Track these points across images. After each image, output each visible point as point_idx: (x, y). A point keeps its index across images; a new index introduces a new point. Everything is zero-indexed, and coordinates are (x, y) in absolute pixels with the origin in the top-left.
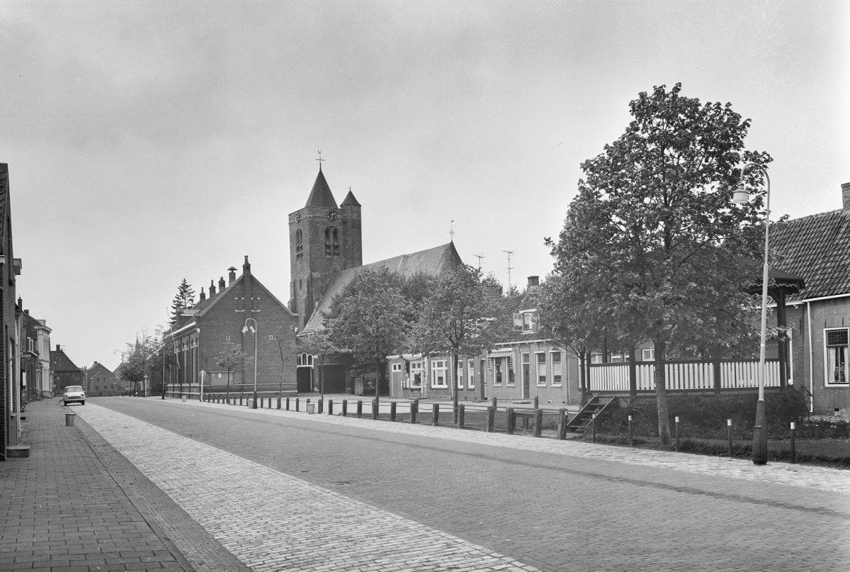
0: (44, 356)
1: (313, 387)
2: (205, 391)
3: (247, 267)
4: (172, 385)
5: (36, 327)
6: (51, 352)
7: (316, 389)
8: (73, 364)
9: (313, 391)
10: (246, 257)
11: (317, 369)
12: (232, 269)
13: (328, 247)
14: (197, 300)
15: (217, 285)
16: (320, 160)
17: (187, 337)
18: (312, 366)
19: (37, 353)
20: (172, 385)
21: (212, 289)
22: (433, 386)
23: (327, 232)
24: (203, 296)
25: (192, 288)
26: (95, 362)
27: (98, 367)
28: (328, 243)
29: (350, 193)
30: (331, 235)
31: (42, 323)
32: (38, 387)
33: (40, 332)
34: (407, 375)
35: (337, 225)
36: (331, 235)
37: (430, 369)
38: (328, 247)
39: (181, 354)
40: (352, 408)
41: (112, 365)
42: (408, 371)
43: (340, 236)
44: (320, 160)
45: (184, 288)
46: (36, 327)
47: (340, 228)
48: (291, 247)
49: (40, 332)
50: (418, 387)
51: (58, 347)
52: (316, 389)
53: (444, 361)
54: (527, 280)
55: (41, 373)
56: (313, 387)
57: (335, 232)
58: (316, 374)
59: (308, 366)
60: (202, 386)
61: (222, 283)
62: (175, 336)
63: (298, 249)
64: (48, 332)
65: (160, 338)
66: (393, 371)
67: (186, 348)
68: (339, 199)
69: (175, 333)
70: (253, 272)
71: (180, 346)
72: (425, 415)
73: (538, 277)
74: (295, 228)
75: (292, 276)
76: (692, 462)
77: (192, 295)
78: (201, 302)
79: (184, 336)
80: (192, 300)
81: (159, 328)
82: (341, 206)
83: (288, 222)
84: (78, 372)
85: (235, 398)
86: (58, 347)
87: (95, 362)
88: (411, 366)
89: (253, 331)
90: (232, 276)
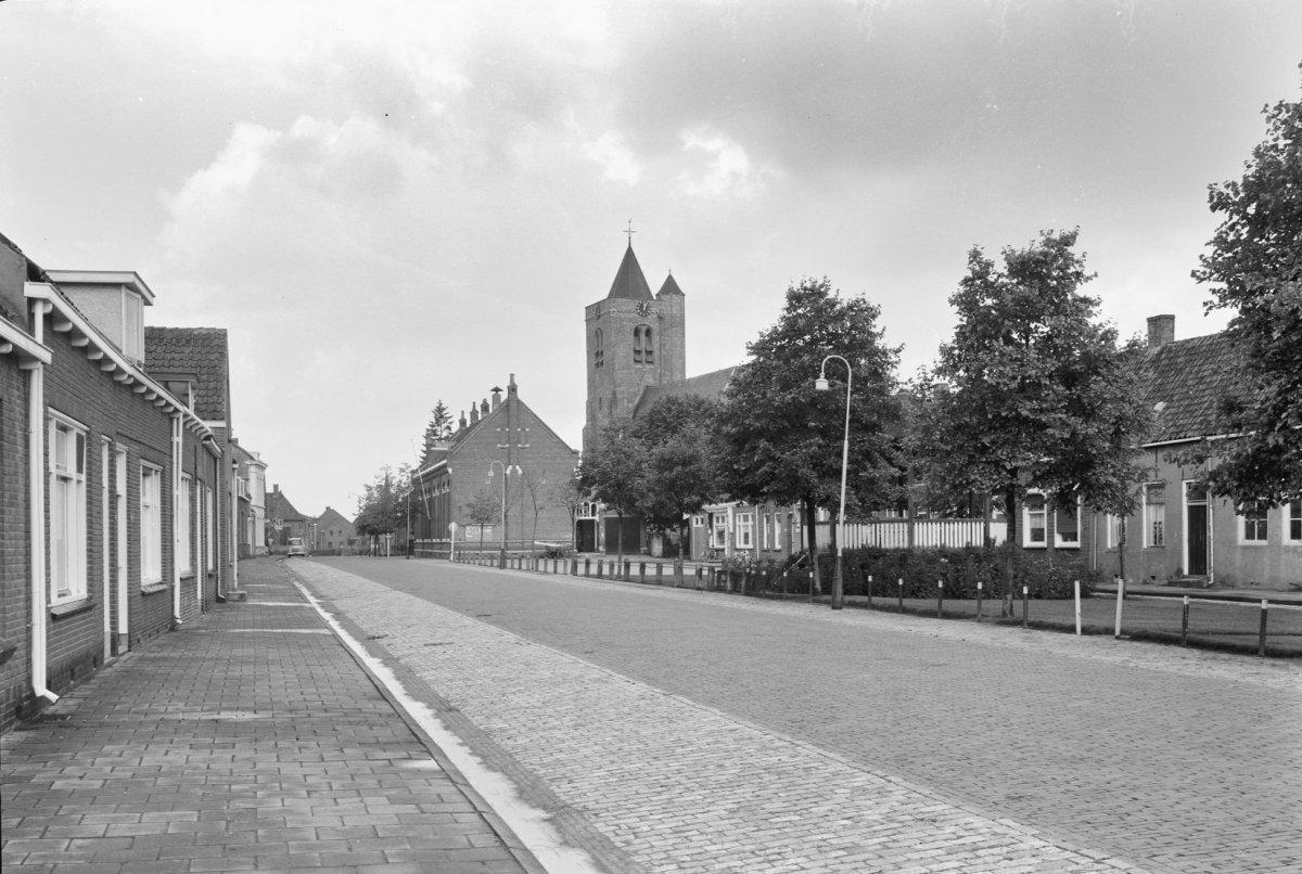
0: (257, 501)
1: (598, 545)
2: (455, 549)
3: (513, 389)
4: (421, 541)
5: (248, 462)
6: (266, 495)
7: (601, 548)
8: (285, 499)
9: (598, 551)
10: (512, 375)
11: (603, 523)
12: (497, 390)
13: (638, 352)
14: (455, 427)
15: (479, 409)
16: (630, 231)
17: (437, 479)
18: (597, 518)
19: (249, 496)
20: (421, 541)
21: (474, 413)
22: (738, 546)
23: (637, 332)
24: (463, 422)
25: (448, 412)
26: (328, 508)
27: (330, 515)
28: (637, 349)
29: (670, 277)
30: (643, 336)
31: (255, 457)
32: (250, 542)
33: (252, 469)
34: (710, 531)
35: (651, 321)
36: (643, 336)
37: (734, 523)
38: (638, 352)
39: (431, 501)
40: (594, 570)
41: (350, 512)
42: (711, 527)
43: (656, 338)
44: (630, 231)
45: (440, 414)
46: (248, 462)
47: (655, 326)
48: (588, 352)
49: (252, 469)
50: (722, 547)
51: (276, 487)
52: (601, 548)
53: (750, 514)
54: (1146, 324)
55: (254, 523)
56: (598, 545)
57: (648, 333)
58: (602, 527)
59: (591, 518)
60: (453, 542)
61: (485, 407)
62: (423, 476)
63: (597, 355)
64: (261, 467)
65: (405, 479)
66: (695, 525)
67: (436, 493)
68: (655, 285)
69: (425, 472)
70: (521, 395)
71: (430, 491)
72: (593, 576)
73: (1171, 318)
74: (594, 326)
75: (589, 394)
76: (1150, 656)
77: (450, 420)
78: (460, 430)
79: (434, 477)
80: (449, 428)
81: (404, 467)
82: (657, 295)
83: (584, 318)
84: (302, 519)
85: (512, 559)
86: (276, 487)
87: (328, 508)
88: (715, 520)
89: (520, 472)
90: (496, 398)
